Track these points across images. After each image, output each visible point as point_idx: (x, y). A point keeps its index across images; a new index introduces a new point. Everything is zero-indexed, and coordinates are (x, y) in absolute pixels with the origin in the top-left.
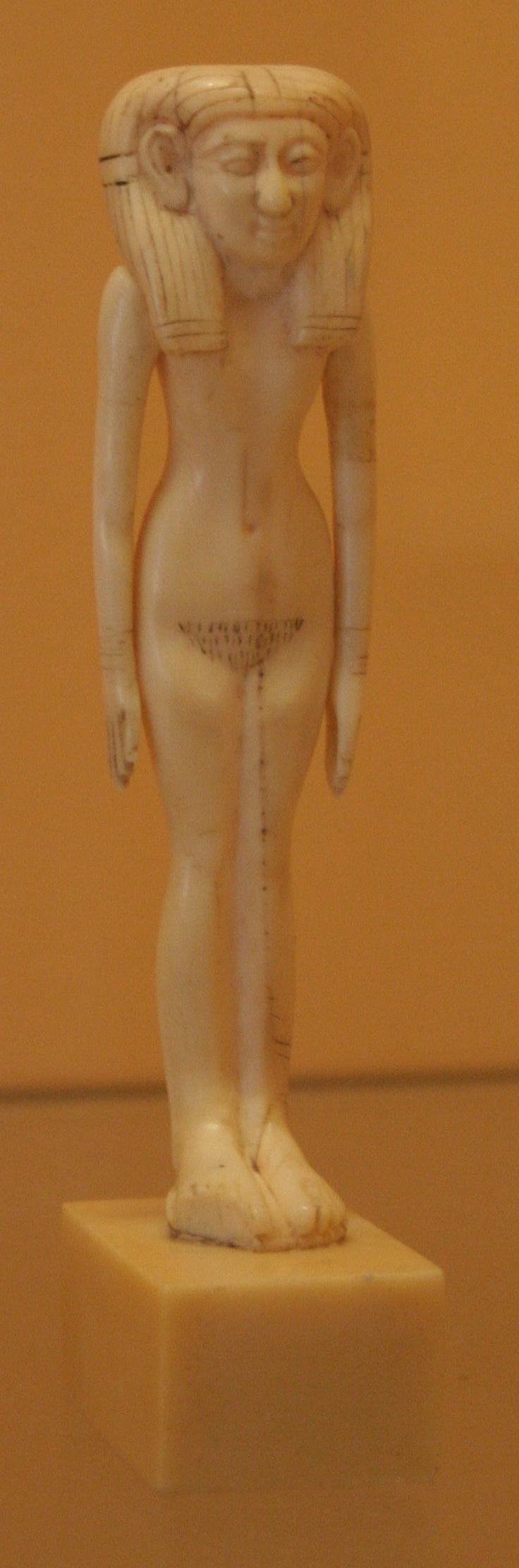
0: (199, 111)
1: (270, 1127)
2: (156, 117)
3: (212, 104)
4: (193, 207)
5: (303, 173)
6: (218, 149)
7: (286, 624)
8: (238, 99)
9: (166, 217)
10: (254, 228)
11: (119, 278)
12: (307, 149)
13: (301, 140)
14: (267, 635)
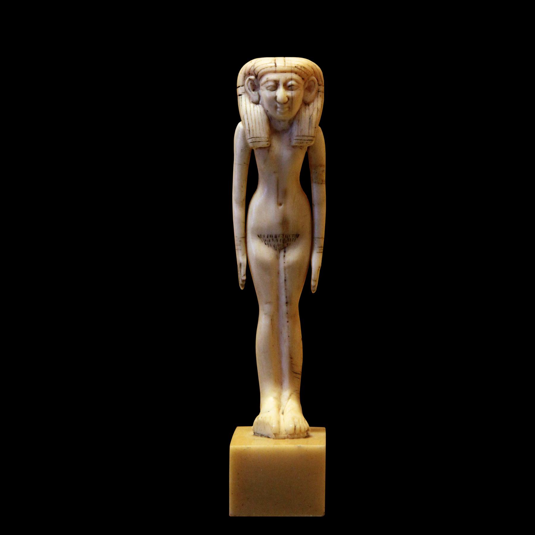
0: (260, 71)
1: (290, 400)
2: (249, 74)
3: (267, 68)
4: (260, 102)
5: (292, 90)
6: (265, 83)
8: (271, 67)
9: (252, 105)
10: (276, 108)
12: (293, 82)
13: (291, 79)
14: (286, 239)
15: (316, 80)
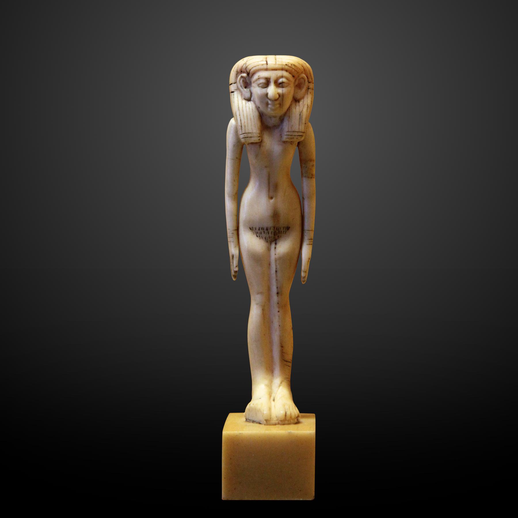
0: (251, 69)
1: (281, 387)
2: (242, 72)
3: (258, 65)
4: (252, 99)
5: (283, 87)
6: (257, 80)
8: (263, 65)
9: (244, 101)
10: (267, 104)
11: (232, 122)
12: (284, 80)
13: (282, 77)
14: (277, 231)
15: (306, 77)
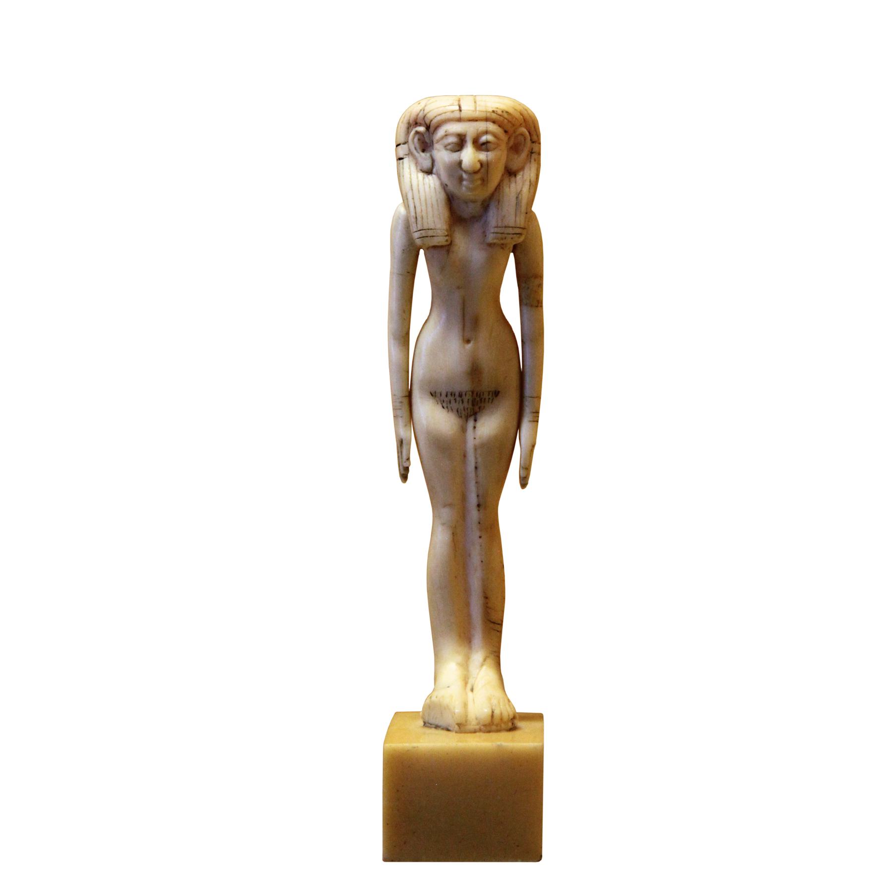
0: (433, 119)
1: (484, 667)
2: (416, 124)
4: (434, 170)
5: (487, 150)
6: (442, 138)
7: (489, 393)
8: (453, 112)
9: (421, 175)
10: (461, 179)
12: (489, 137)
13: (486, 132)
14: (478, 399)
15: (528, 133)
